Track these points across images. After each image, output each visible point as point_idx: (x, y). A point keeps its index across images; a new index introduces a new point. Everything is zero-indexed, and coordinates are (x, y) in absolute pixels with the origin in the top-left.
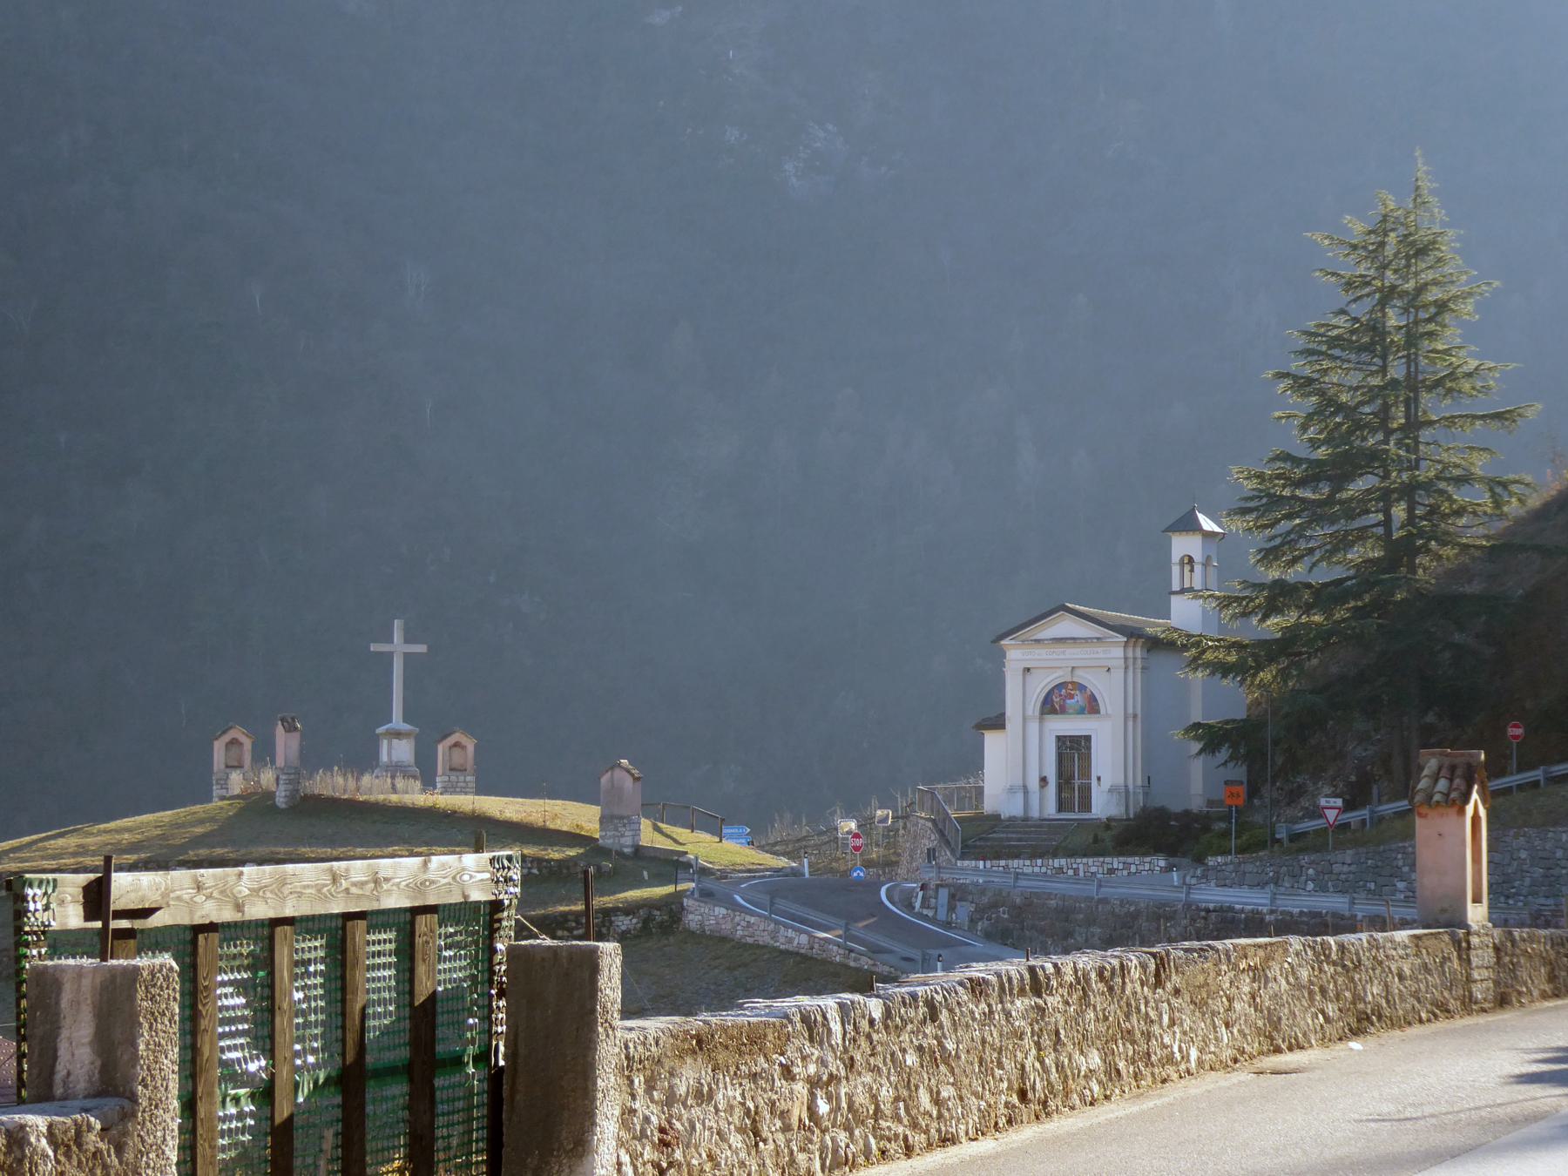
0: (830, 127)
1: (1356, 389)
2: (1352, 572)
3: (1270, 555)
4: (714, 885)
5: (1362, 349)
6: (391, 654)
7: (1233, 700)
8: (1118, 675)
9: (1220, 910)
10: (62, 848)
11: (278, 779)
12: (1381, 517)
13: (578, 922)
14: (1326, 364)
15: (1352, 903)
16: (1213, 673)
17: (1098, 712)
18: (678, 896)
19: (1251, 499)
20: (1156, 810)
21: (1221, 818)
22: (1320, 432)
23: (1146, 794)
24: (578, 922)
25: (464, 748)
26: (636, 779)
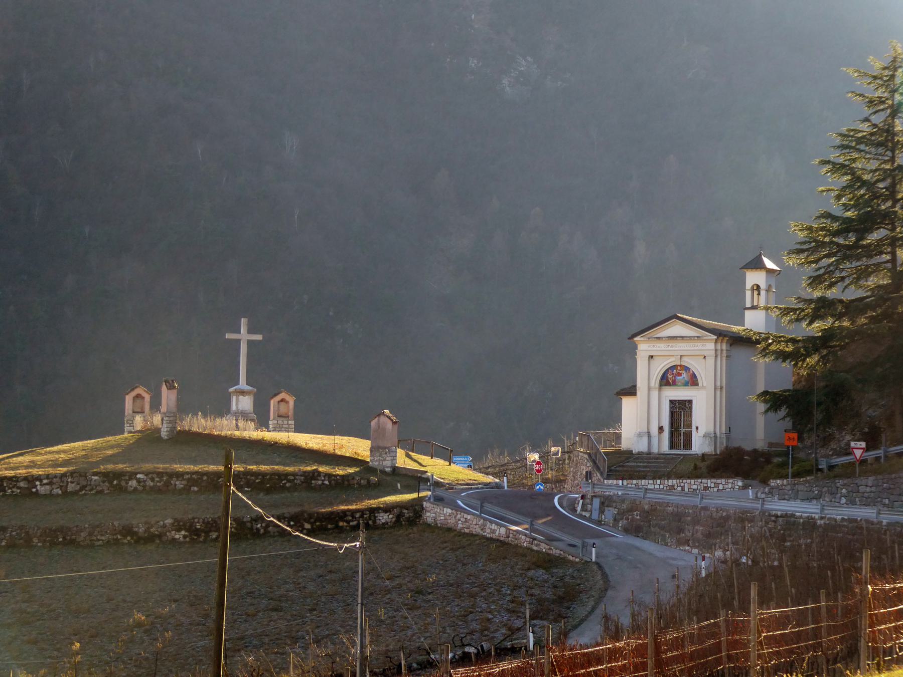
0: (529, 59)
1: (876, 170)
2: (869, 293)
3: (816, 281)
4: (444, 492)
5: (879, 145)
6: (239, 341)
7: (785, 377)
8: (711, 361)
9: (785, 516)
10: (20, 463)
11: (162, 419)
12: (888, 257)
13: (353, 517)
14: (855, 155)
15: (879, 513)
16: (777, 358)
17: (697, 384)
18: (420, 500)
19: (804, 243)
20: (735, 448)
21: (779, 455)
22: (850, 200)
23: (728, 439)
24: (353, 517)
25: (287, 402)
26: (394, 423)
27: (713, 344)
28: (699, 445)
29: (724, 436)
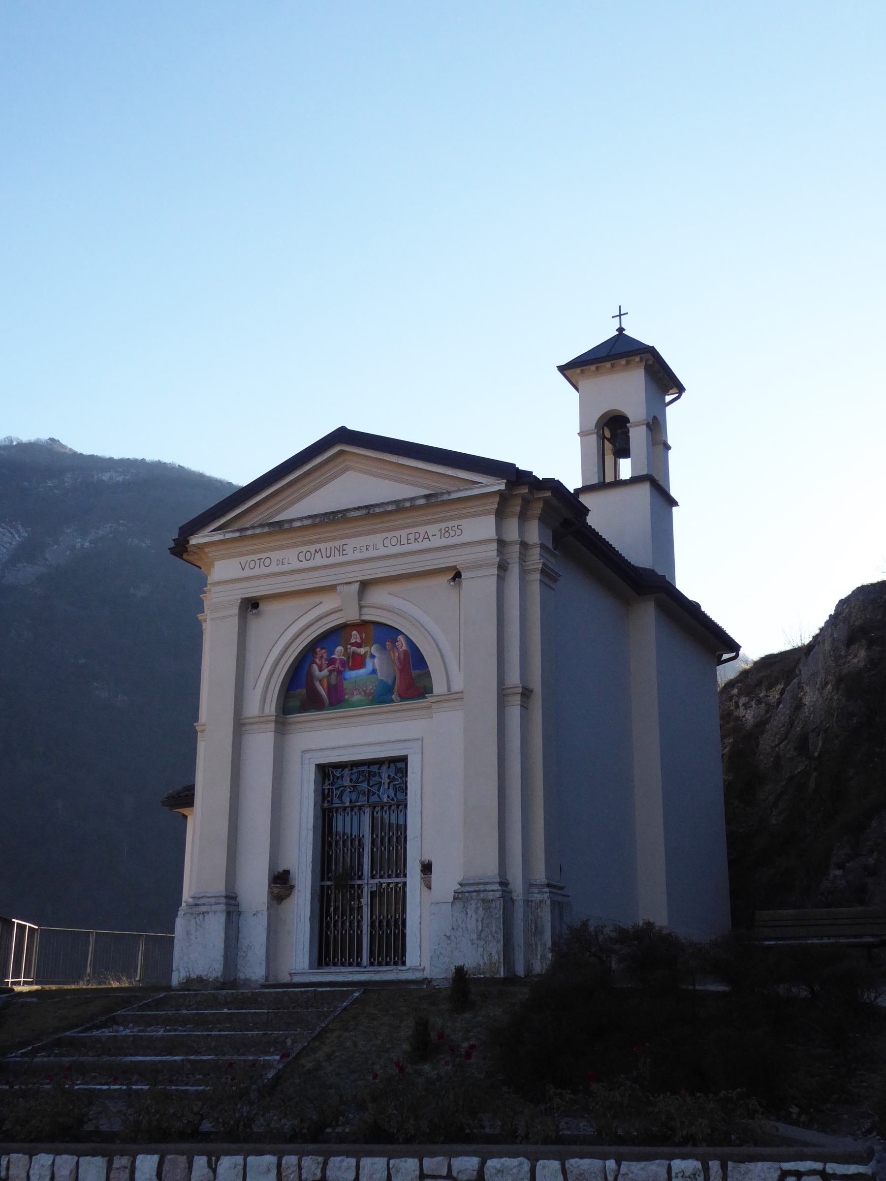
8: (481, 587)
9: (435, 1143)
23: (559, 908)
27: (491, 520)
28: (435, 939)
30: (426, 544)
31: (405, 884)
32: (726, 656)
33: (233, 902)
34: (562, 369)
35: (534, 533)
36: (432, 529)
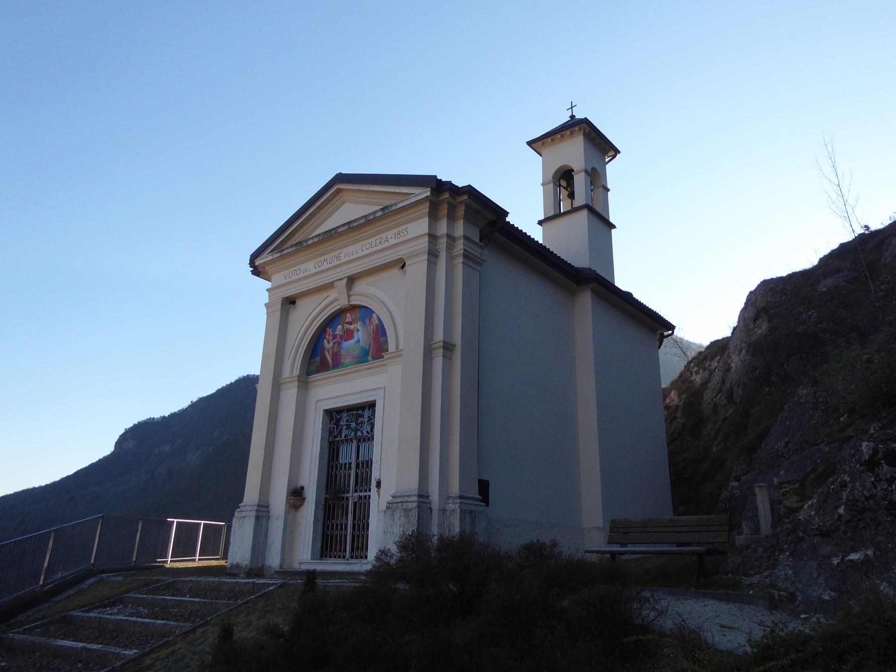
8: (418, 269)
29: (454, 506)
30: (387, 244)
31: (370, 497)
32: (666, 334)
33: (264, 509)
34: (530, 143)
35: (460, 229)
36: (390, 234)
